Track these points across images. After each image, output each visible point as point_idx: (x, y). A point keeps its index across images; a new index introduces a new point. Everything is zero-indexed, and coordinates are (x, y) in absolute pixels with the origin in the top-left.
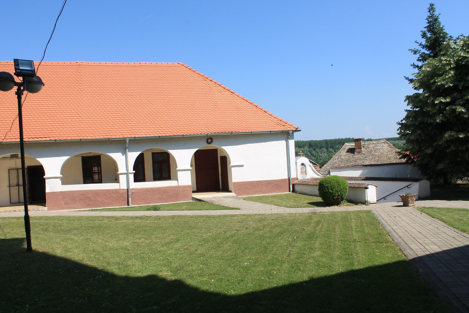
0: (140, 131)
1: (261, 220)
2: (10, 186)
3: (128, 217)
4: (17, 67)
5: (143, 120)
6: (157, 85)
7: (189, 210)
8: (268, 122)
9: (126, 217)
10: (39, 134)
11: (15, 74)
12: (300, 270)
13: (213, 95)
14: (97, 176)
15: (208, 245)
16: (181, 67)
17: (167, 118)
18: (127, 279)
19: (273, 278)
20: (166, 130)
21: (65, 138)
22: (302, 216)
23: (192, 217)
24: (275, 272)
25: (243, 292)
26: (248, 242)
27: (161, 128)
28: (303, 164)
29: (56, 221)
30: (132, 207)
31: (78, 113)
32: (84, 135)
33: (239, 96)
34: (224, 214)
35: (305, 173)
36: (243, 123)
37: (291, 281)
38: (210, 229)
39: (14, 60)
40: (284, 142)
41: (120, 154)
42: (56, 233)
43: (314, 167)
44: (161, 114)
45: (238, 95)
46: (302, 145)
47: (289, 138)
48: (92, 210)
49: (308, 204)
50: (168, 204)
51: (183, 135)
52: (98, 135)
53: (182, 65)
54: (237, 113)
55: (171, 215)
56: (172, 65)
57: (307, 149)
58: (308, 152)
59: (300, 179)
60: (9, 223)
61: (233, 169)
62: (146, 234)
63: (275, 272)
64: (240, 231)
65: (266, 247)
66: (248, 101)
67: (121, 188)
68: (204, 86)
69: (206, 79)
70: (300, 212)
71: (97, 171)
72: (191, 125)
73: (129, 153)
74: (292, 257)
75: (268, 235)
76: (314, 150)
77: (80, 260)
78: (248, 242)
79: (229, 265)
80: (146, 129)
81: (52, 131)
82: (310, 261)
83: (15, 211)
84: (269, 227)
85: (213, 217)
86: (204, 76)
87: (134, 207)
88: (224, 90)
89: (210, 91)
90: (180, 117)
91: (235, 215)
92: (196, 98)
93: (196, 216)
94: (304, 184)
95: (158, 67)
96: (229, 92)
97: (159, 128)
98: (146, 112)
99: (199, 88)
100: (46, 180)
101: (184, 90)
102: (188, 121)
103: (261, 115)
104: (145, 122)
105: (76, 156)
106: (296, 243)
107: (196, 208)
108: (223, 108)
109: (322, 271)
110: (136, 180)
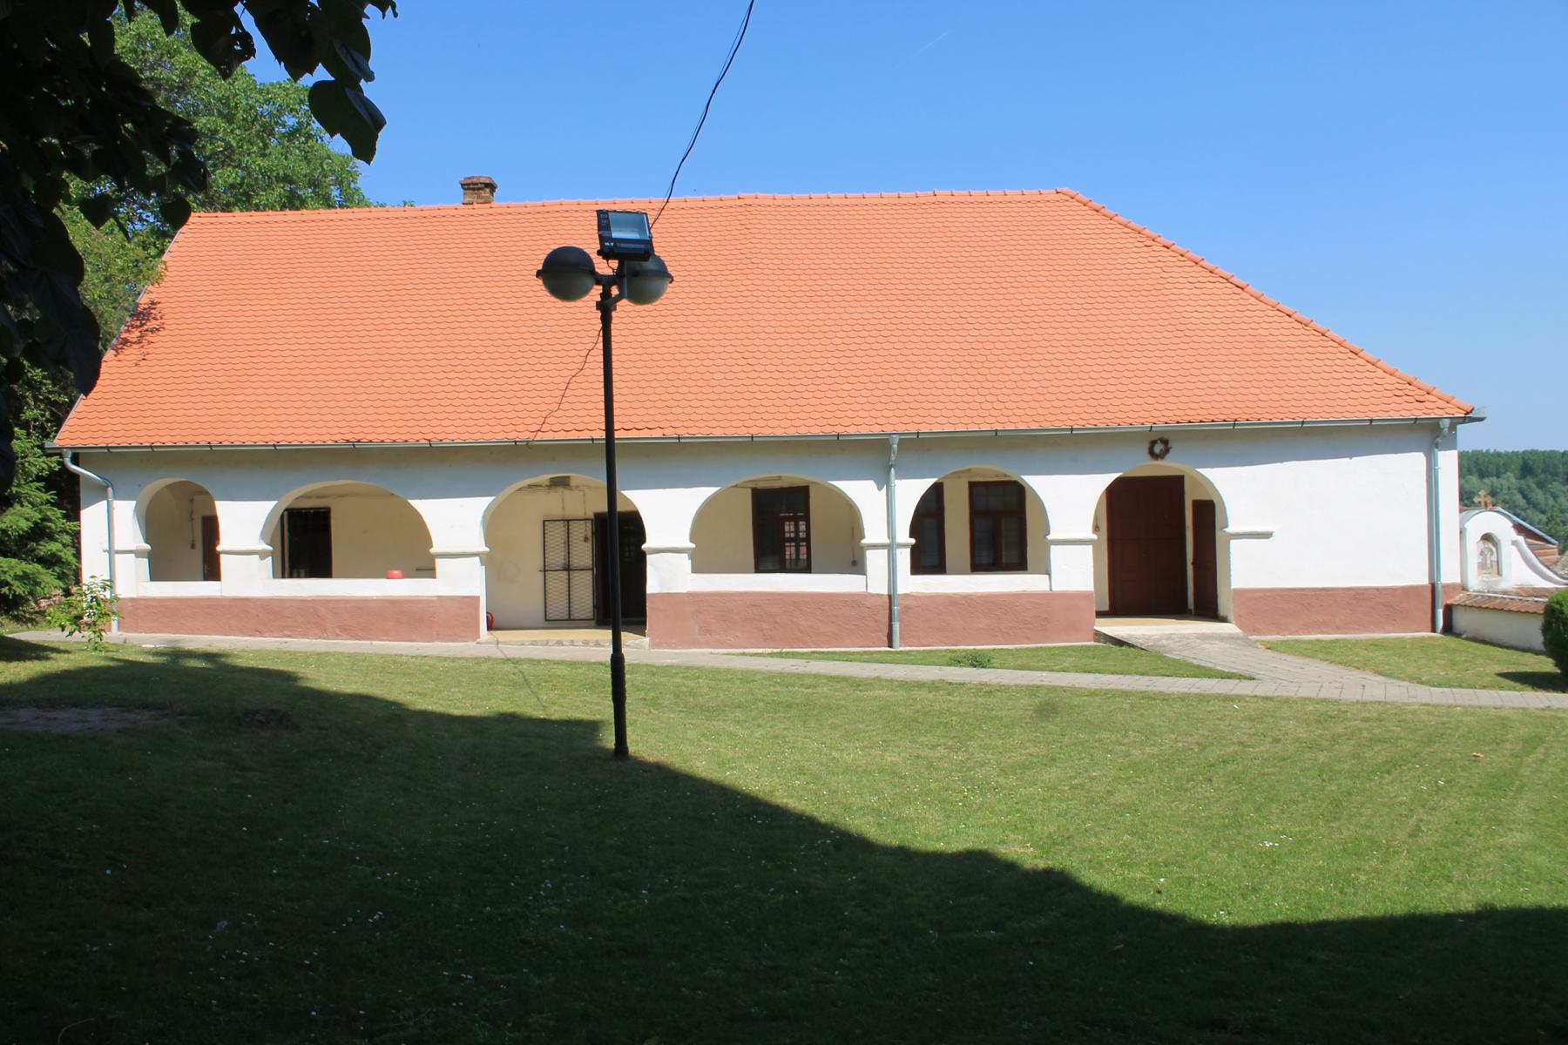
0: (933, 412)
1: (1324, 719)
2: (545, 571)
3: (892, 681)
4: (606, 234)
5: (944, 378)
6: (988, 264)
7: (1085, 672)
8: (1364, 387)
9: (886, 681)
10: (633, 419)
11: (599, 253)
12: (1448, 879)
13: (1172, 297)
14: (793, 549)
15: (1147, 780)
16: (1067, 203)
17: (1021, 371)
18: (904, 854)
19: (1355, 894)
20: (1017, 412)
21: (705, 432)
22: (1473, 714)
23: (1093, 693)
24: (1363, 878)
25: (1257, 920)
26: (1278, 781)
27: (1001, 406)
28: (1487, 538)
29: (678, 680)
30: (901, 652)
31: (746, 355)
32: (762, 423)
33: (1261, 298)
34: (1198, 691)
35: (1495, 567)
36: (1275, 390)
37: (1416, 907)
38: (1155, 735)
39: (599, 212)
40: (1417, 459)
41: (870, 485)
42: (683, 714)
43: (1532, 548)
44: (1003, 358)
45: (1257, 295)
46: (1492, 468)
47: (1437, 446)
48: (780, 655)
49: (1499, 679)
50: (1017, 650)
51: (1072, 430)
52: (806, 422)
53: (1068, 198)
54: (1253, 357)
55: (1026, 683)
56: (1039, 198)
57: (1513, 480)
58: (1515, 491)
59: (1475, 588)
60: (550, 676)
61: (1234, 543)
62: (952, 735)
63: (1363, 878)
64: (1253, 747)
65: (1336, 804)
66: (1294, 316)
67: (871, 590)
68: (1142, 266)
69: (1149, 243)
70: (1467, 703)
71: (793, 535)
72: (1100, 396)
73: (897, 482)
74: (1425, 840)
75: (1346, 766)
76: (1540, 485)
77: (765, 793)
78: (1278, 781)
79: (1215, 845)
80: (953, 406)
81: (668, 410)
82: (1488, 857)
83: (560, 643)
84: (1352, 742)
85: (1164, 697)
86: (1144, 232)
87: (907, 653)
88: (1211, 279)
89: (1165, 281)
90: (1062, 369)
91: (1237, 696)
92: (1117, 305)
93: (1107, 692)
94: (1488, 606)
95: (990, 205)
96: (1228, 285)
97: (995, 405)
98: (954, 353)
99: (1125, 271)
100: (649, 557)
101: (1076, 278)
102: (1089, 382)
103: (1338, 362)
104: (951, 385)
105: (736, 486)
106: (1444, 798)
107: (1106, 665)
108: (1206, 339)
109: (1528, 892)
110: (918, 567)
